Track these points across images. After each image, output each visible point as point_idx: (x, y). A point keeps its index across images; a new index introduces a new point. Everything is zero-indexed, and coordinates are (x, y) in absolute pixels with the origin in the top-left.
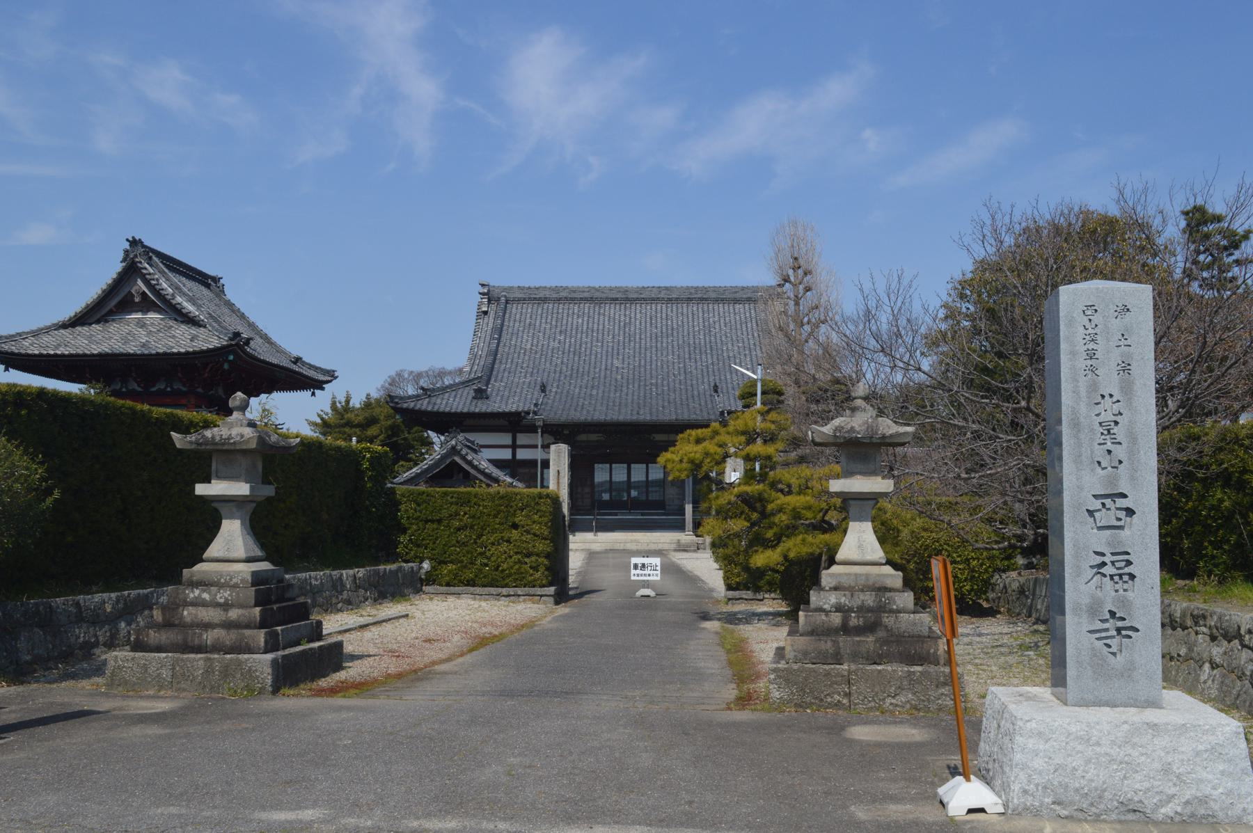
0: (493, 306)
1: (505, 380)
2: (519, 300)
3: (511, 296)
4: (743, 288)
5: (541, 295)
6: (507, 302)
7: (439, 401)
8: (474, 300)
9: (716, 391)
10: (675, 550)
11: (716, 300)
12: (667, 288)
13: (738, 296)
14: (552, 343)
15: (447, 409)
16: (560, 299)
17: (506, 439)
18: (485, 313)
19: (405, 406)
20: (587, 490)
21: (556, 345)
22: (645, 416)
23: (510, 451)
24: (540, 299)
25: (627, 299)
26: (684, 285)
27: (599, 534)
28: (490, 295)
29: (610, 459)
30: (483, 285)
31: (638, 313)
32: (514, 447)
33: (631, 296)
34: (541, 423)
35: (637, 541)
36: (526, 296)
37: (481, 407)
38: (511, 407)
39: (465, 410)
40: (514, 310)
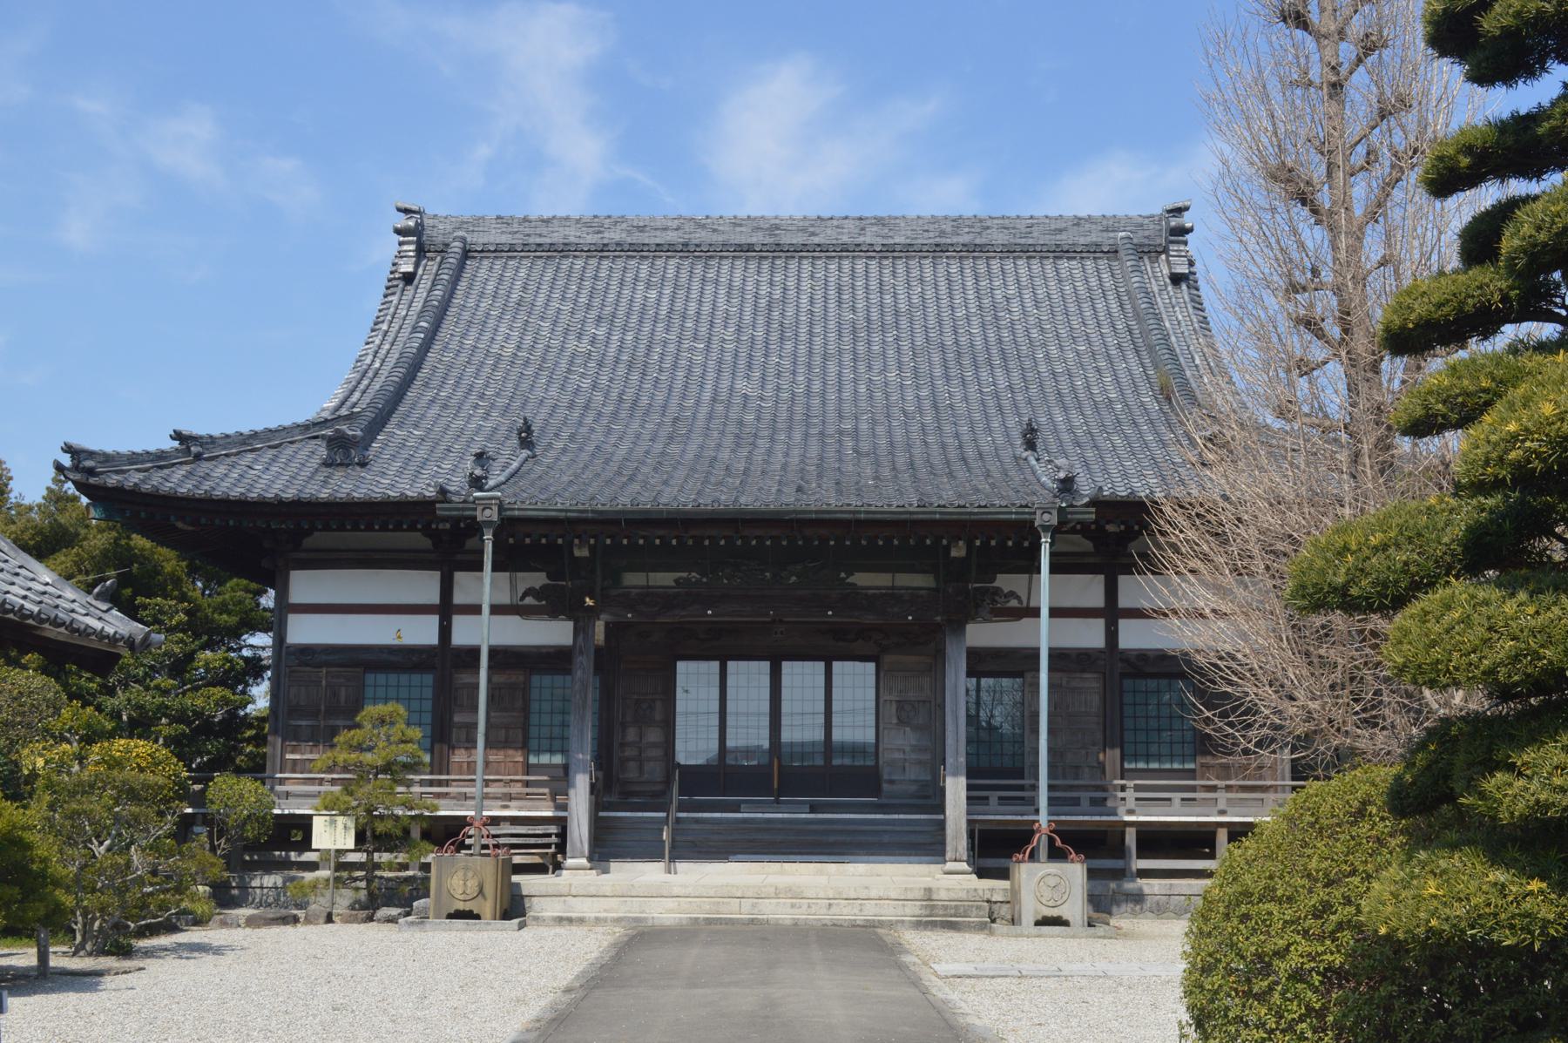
0: (432, 266)
1: (425, 424)
2: (498, 251)
3: (478, 239)
4: (1078, 221)
5: (557, 238)
6: (466, 254)
7: (221, 470)
8: (385, 251)
9: (1031, 445)
10: (919, 925)
11: (1009, 251)
12: (880, 221)
13: (1065, 239)
14: (572, 343)
15: (236, 493)
16: (603, 248)
17: (423, 586)
18: (409, 278)
19: (113, 480)
20: (654, 735)
21: (584, 346)
22: (824, 498)
23: (434, 620)
24: (552, 248)
25: (778, 249)
26: (927, 213)
27: (682, 866)
28: (418, 236)
29: (723, 647)
30: (406, 211)
31: (804, 277)
32: (446, 610)
33: (786, 239)
34: (492, 514)
35: (794, 894)
36: (517, 240)
37: (347, 486)
38: (418, 487)
39: (290, 494)
40: (483, 273)
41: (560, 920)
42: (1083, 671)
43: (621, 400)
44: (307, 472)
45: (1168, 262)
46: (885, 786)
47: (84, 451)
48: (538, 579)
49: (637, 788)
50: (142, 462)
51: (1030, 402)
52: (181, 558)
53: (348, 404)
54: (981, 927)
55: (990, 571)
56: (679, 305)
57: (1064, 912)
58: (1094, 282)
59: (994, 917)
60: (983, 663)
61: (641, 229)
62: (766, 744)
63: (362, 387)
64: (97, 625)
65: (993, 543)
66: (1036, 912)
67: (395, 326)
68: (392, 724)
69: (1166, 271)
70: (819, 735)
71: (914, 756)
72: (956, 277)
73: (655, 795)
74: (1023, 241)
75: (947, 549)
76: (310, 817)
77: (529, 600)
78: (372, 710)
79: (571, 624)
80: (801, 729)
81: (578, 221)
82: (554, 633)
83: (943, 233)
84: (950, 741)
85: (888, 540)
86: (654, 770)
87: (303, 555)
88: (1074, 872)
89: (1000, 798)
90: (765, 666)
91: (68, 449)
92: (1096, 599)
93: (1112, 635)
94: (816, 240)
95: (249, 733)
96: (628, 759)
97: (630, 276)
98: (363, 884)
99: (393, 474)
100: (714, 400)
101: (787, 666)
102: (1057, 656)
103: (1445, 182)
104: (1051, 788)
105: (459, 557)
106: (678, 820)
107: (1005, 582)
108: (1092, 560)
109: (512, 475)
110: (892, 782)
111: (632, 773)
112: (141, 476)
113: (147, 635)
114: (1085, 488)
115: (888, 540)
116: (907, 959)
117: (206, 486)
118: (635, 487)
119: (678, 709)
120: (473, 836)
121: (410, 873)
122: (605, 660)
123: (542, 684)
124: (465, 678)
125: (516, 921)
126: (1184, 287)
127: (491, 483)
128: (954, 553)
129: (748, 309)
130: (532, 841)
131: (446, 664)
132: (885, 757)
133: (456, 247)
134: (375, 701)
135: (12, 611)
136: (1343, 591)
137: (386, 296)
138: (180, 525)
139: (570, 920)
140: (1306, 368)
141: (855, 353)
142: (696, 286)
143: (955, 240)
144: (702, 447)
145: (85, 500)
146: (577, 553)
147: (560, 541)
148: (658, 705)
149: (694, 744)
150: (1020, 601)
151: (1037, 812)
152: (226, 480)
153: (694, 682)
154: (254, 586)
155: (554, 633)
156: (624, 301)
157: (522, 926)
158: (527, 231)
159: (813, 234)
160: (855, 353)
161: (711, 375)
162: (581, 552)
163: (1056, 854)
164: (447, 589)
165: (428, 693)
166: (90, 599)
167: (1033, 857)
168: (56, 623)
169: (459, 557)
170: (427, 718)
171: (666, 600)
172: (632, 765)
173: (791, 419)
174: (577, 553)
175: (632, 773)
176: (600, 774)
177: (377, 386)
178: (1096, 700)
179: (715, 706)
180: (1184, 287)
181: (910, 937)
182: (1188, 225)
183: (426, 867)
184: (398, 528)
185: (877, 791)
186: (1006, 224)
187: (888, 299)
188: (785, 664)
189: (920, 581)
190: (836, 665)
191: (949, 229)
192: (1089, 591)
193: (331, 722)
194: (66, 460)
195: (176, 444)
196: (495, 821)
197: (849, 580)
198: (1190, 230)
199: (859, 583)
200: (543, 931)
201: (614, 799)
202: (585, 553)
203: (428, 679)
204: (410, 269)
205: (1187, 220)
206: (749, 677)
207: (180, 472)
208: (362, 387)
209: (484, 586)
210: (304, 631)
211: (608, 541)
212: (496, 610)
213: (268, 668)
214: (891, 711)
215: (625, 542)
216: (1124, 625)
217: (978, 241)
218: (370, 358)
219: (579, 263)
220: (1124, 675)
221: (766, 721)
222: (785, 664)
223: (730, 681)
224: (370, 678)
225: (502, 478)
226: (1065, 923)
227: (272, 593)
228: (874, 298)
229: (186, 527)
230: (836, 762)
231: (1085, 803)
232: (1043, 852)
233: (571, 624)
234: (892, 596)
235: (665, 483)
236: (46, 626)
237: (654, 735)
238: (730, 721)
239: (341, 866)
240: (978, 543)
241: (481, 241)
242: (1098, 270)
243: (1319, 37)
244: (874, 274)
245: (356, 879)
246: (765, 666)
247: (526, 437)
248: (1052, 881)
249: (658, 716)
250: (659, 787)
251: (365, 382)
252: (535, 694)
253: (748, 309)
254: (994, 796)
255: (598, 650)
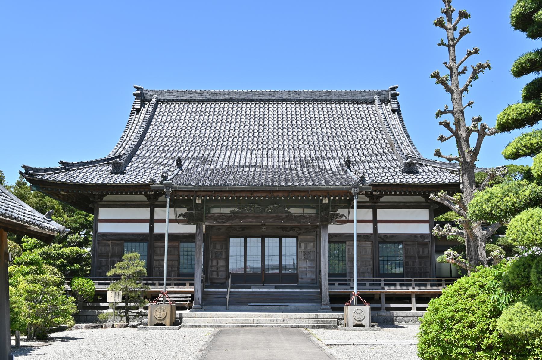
6: (158, 102)
7: (77, 174)
9: (349, 167)
10: (314, 327)
11: (339, 101)
17: (144, 213)
18: (138, 111)
24: (185, 101)
29: (245, 233)
32: (152, 221)
37: (119, 179)
38: (144, 179)
39: (99, 182)
41: (192, 326)
42: (366, 241)
43: (210, 151)
44: (105, 175)
45: (391, 105)
46: (300, 280)
47: (29, 167)
48: (184, 211)
49: (216, 281)
50: (50, 171)
51: (347, 151)
52: (60, 204)
53: (119, 152)
54: (335, 328)
55: (335, 208)
56: (229, 120)
57: (363, 323)
58: (367, 112)
59: (339, 324)
60: (334, 239)
61: (216, 94)
62: (260, 266)
63: (123, 146)
64: (48, 226)
65: (337, 198)
66: (354, 322)
67: (134, 126)
68: (135, 260)
69: (390, 108)
70: (278, 263)
71: (309, 270)
72: (321, 110)
73: (222, 283)
74: (343, 98)
75: (322, 200)
76: (106, 291)
77: (181, 218)
78: (126, 256)
79: (195, 226)
80: (272, 260)
81: (195, 92)
82: (190, 229)
83: (316, 96)
84: (323, 264)
85: (302, 197)
86: (222, 275)
87: (103, 203)
88: (366, 309)
89: (339, 284)
90: (260, 239)
91: (24, 167)
92: (370, 217)
93: (375, 229)
94: (274, 98)
95: (84, 263)
96: (213, 271)
97: (212, 110)
98: (124, 314)
99: (134, 175)
100: (242, 151)
101: (267, 240)
102: (359, 236)
103: (520, 71)
104: (358, 280)
105: (156, 203)
106: (231, 291)
107: (340, 211)
108: (368, 204)
109: (175, 176)
110: (302, 278)
111: (214, 276)
112: (49, 176)
113: (64, 229)
114: (368, 181)
115: (302, 197)
116: (313, 338)
117: (71, 179)
118: (217, 180)
119: (230, 254)
120: (160, 297)
121: (139, 311)
122: (206, 238)
123: (184, 246)
124: (159, 244)
125: (178, 326)
126: (396, 113)
127: (169, 178)
128: (324, 202)
129: (252, 121)
130: (181, 299)
131: (152, 240)
132: (300, 270)
133: (154, 100)
134: (127, 252)
135: (21, 220)
136: (490, 213)
137: (130, 116)
138: (62, 192)
139: (196, 326)
140: (442, 139)
141: (288, 135)
142: (234, 113)
143: (320, 98)
144: (238, 166)
145: (29, 184)
146: (197, 202)
147: (192, 198)
148: (223, 253)
149: (235, 265)
150: (346, 218)
151: (353, 288)
152: (77, 177)
153: (236, 245)
154: (84, 213)
155: (190, 229)
156: (211, 118)
157: (179, 328)
158: (178, 95)
159: (273, 96)
160: (288, 135)
161: (240, 142)
162: (199, 201)
163: (360, 303)
164: (152, 214)
165: (146, 249)
166: (44, 216)
167: (353, 304)
168: (34, 224)
169: (156, 203)
170: (146, 257)
171: (228, 218)
172: (215, 273)
173: (267, 157)
174: (197, 202)
175: (214, 276)
176: (204, 276)
177: (128, 146)
178: (370, 251)
179: (243, 253)
180: (396, 113)
181: (315, 331)
182: (398, 93)
183: (146, 308)
184: (136, 194)
185: (297, 281)
186: (337, 93)
187: (299, 117)
188: (266, 239)
189: (314, 211)
190: (283, 239)
191: (318, 95)
192: (368, 214)
193: (113, 259)
194: (23, 171)
195: (61, 165)
196: (169, 292)
197: (289, 211)
198: (398, 95)
199: (292, 212)
200: (186, 329)
201: (209, 284)
202: (200, 202)
203: (145, 244)
204: (139, 107)
205: (397, 91)
206: (254, 243)
207: (62, 175)
208: (123, 146)
209: (166, 213)
210: (103, 228)
211: (208, 198)
212: (171, 221)
213: (90, 241)
214: (301, 255)
215: (214, 198)
216: (379, 225)
217: (328, 98)
218: (125, 137)
219: (195, 105)
220: (379, 242)
221: (260, 258)
222: (266, 239)
223: (248, 245)
224: (126, 244)
225: (172, 177)
226: (364, 326)
227: (93, 216)
228: (294, 117)
229: (64, 193)
230: (283, 272)
231: (367, 285)
232: (356, 302)
233: (195, 226)
234: (303, 216)
235: (227, 178)
236: (32, 226)
237: (222, 263)
238: (248, 258)
239: (118, 308)
240: (332, 198)
241: (162, 98)
242: (368, 108)
243: (446, 29)
244: (294, 109)
245: (122, 312)
246: (260, 239)
247: (179, 163)
248: (359, 312)
249: (223, 257)
250: (224, 281)
251: (124, 145)
252: (182, 249)
253: (252, 121)
254: (337, 283)
255: (204, 234)
